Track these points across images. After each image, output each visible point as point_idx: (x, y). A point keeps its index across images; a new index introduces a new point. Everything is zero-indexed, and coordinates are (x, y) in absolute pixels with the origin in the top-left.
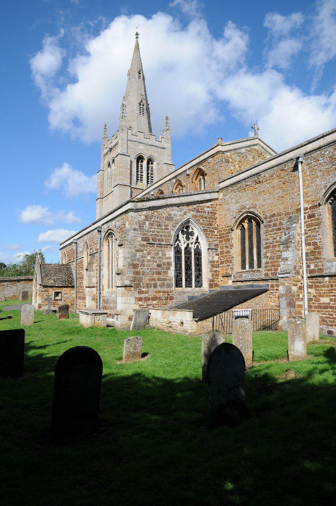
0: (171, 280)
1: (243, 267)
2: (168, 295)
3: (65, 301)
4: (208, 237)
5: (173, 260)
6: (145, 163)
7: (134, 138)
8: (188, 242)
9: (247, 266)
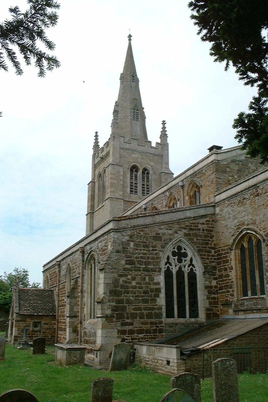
0: (160, 308)
1: (245, 294)
2: (156, 327)
3: (44, 332)
4: (204, 258)
5: (162, 285)
6: (140, 173)
7: (127, 146)
8: (180, 264)
9: (249, 293)
